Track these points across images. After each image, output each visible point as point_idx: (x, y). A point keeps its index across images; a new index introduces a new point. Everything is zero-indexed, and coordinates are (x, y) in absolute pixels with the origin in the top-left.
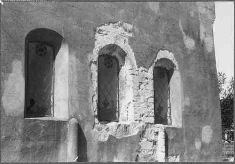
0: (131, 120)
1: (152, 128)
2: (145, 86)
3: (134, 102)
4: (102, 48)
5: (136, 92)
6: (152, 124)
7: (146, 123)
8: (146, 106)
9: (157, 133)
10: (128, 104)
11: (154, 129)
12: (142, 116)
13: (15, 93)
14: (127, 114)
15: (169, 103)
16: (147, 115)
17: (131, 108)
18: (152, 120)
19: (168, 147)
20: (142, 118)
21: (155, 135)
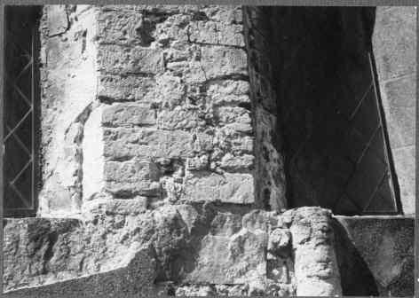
0: (92, 198)
1: (243, 232)
2: (182, 25)
3: (105, 107)
4: (366, 265)
5: (119, 54)
6: (242, 208)
7: (197, 206)
8: (192, 119)
9: (285, 254)
10: (78, 120)
11: (258, 232)
12: (169, 168)
13: (290, 272)
14: (73, 166)
15: (385, 146)
16: (201, 160)
17: (94, 130)
18: (242, 188)
19: (398, 186)
20: (169, 182)
21: (270, 265)
